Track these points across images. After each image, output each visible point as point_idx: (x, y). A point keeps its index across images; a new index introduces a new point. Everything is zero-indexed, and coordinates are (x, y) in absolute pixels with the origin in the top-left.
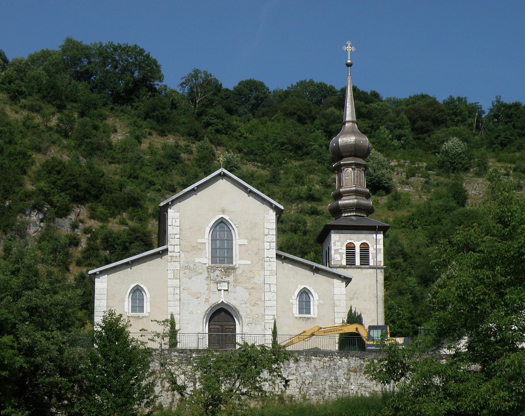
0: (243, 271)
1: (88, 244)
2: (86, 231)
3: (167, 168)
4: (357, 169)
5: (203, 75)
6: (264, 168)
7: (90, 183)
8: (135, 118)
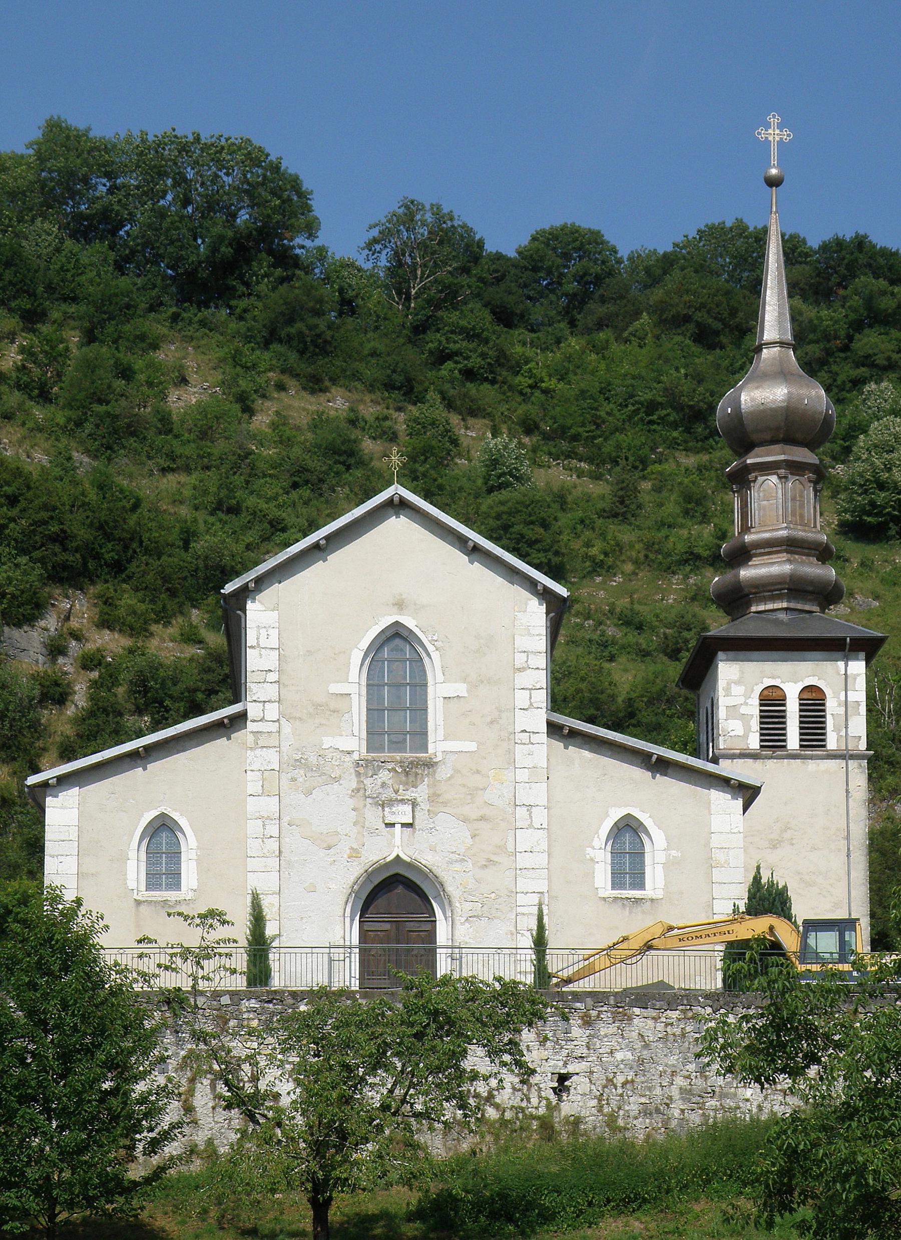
0: (457, 771)
1: (92, 699)
2: (89, 662)
3: (321, 481)
4: (792, 478)
5: (429, 218)
7: (101, 527)
8: (238, 343)
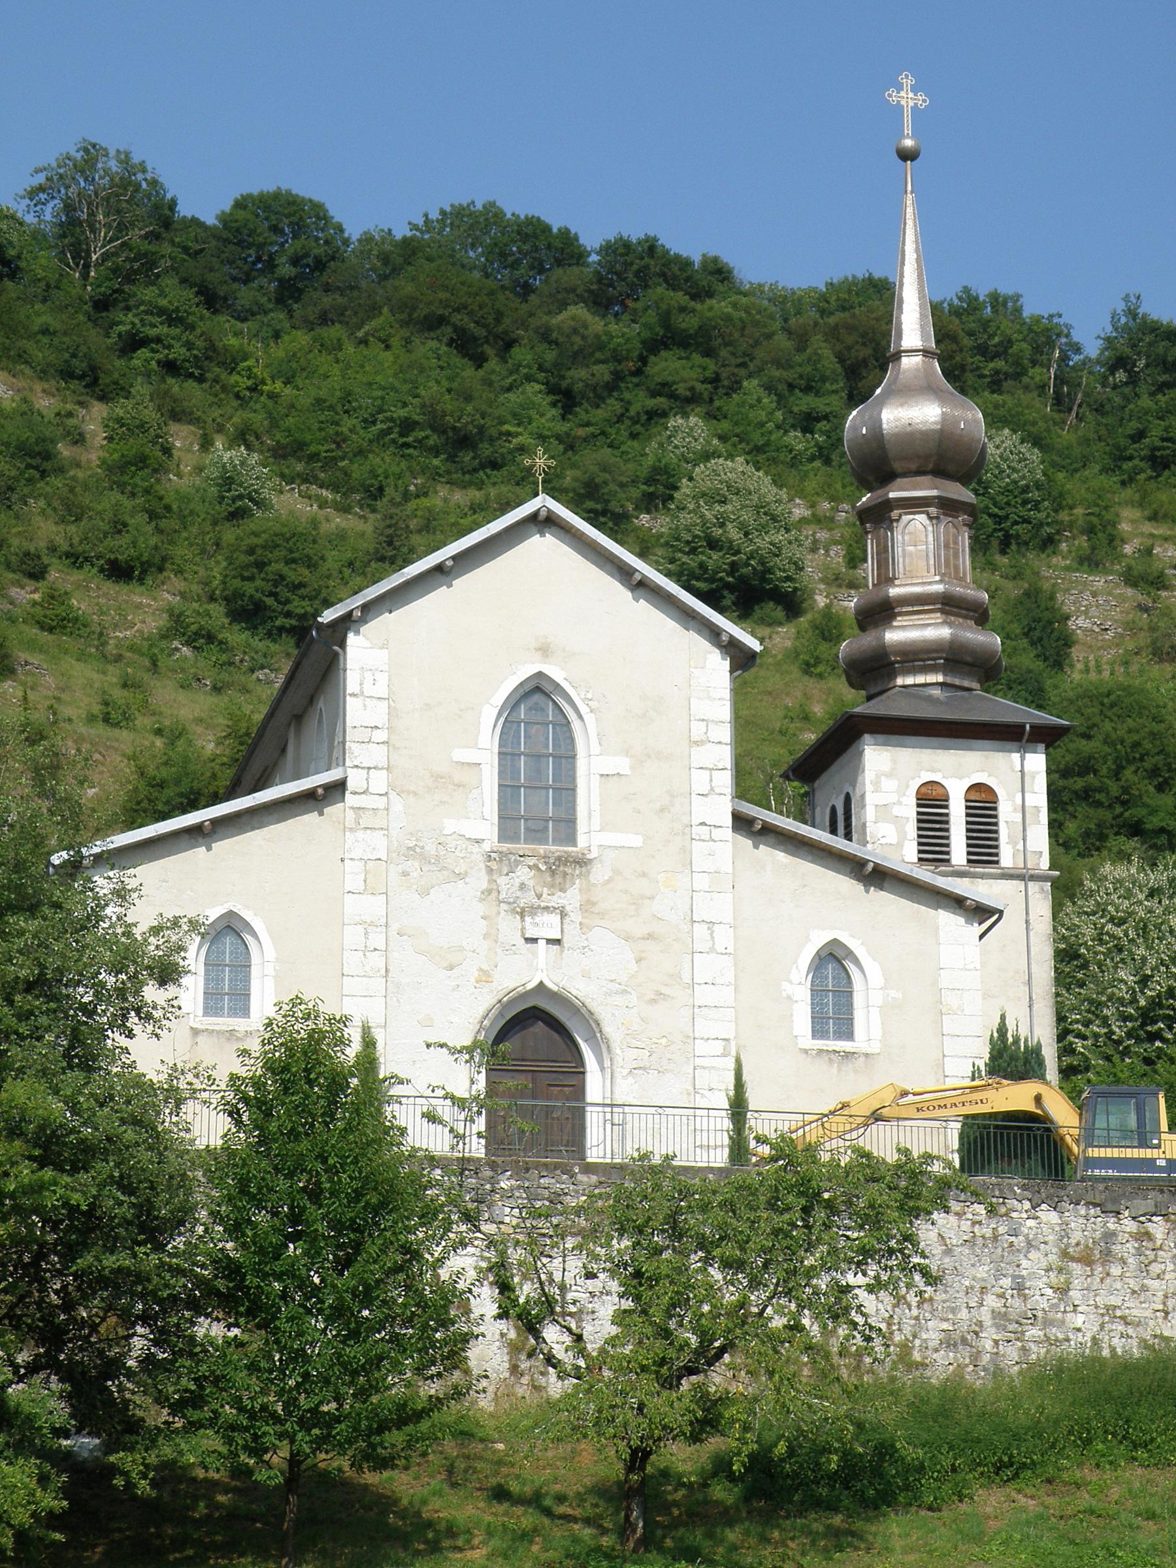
0: (617, 872)
5: (113, 165)
6: (345, 510)
